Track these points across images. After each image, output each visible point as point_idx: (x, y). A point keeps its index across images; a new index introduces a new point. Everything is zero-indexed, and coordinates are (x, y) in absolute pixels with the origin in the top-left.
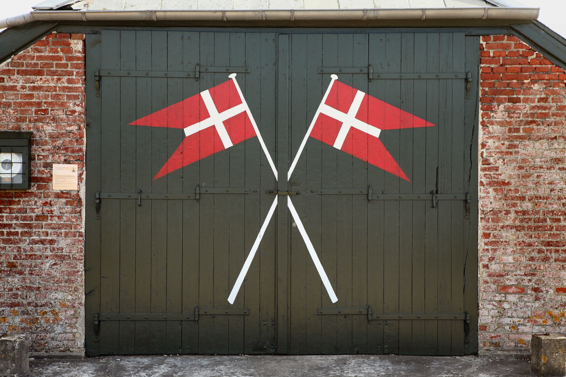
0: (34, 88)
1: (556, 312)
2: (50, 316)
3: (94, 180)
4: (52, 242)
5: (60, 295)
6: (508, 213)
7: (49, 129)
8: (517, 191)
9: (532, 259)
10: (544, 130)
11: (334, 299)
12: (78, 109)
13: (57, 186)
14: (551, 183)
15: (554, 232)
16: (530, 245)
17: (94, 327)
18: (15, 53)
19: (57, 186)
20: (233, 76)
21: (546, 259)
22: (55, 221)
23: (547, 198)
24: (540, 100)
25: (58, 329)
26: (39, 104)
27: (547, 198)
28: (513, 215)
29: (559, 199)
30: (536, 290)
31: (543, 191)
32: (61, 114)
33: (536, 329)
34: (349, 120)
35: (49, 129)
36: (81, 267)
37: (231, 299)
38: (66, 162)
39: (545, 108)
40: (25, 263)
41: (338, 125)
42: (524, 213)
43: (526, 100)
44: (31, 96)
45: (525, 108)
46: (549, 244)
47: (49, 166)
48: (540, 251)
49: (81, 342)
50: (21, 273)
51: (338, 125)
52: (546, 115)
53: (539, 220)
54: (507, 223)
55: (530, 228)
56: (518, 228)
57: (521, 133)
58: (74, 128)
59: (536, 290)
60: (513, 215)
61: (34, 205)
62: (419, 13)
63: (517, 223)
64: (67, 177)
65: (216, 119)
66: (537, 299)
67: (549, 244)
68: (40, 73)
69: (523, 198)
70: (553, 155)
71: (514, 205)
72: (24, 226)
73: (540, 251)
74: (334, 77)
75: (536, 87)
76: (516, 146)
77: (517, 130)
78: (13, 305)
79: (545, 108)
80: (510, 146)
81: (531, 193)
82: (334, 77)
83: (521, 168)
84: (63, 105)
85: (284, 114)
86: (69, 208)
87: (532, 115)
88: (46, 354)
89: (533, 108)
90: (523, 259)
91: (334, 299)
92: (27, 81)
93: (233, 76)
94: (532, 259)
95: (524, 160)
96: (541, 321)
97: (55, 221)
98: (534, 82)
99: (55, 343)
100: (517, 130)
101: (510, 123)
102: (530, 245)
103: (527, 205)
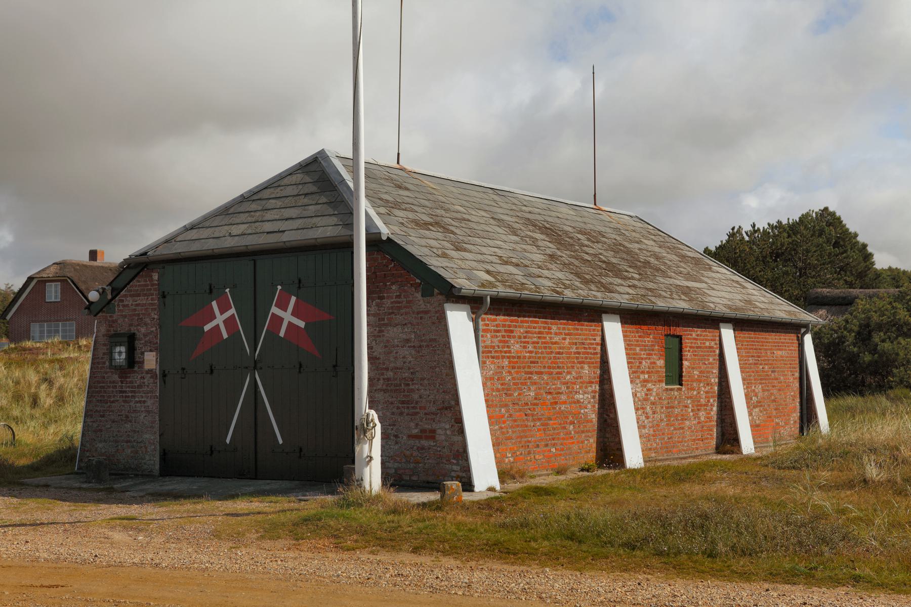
0: (137, 305)
1: (408, 453)
2: (143, 449)
3: (162, 361)
4: (144, 402)
5: (147, 436)
6: (379, 380)
7: (143, 330)
8: (384, 364)
9: (393, 413)
10: (399, 318)
11: (281, 442)
12: (156, 317)
13: (147, 366)
14: (404, 357)
15: (406, 393)
16: (392, 403)
17: (164, 455)
18: (128, 284)
19: (147, 366)
20: (227, 290)
21: (401, 414)
22: (145, 389)
23: (401, 369)
24: (397, 297)
25: (147, 458)
26: (139, 315)
27: (401, 369)
28: (381, 381)
29: (409, 369)
30: (396, 436)
31: (399, 364)
32: (148, 320)
33: (396, 465)
34: (287, 317)
35: (143, 330)
36: (157, 418)
37: (228, 441)
38: (151, 351)
39: (399, 303)
40: (133, 415)
41: (282, 320)
42: (388, 379)
43: (388, 297)
44: (135, 310)
45: (387, 303)
46: (403, 402)
47: (143, 353)
48: (398, 408)
49: (157, 467)
50: (131, 422)
51: (282, 320)
52: (399, 308)
53: (396, 385)
54: (379, 387)
55: (391, 390)
56: (385, 391)
57: (386, 321)
58: (154, 329)
59: (396, 436)
60: (381, 381)
61: (135, 378)
62: (313, 241)
63: (384, 387)
64: (150, 360)
65: (287, 317)
66: (397, 443)
67: (403, 402)
68: (139, 295)
69: (387, 369)
70: (404, 336)
71: (383, 374)
72: (132, 392)
73: (398, 408)
74: (279, 287)
75: (394, 287)
76: (383, 331)
77: (383, 319)
78: (127, 442)
79: (399, 303)
80: (380, 331)
81: (392, 365)
82: (279, 287)
83: (386, 347)
84: (149, 314)
85: (254, 315)
86: (152, 380)
87: (392, 307)
88: (704, 452)
89: (392, 303)
90: (388, 414)
91: (281, 442)
92: (134, 301)
93: (227, 290)
94: (393, 413)
95: (388, 341)
96: (398, 459)
97: (145, 389)
98: (393, 284)
99: (145, 467)
100: (383, 319)
101: (379, 314)
102: (392, 403)
103: (390, 374)
